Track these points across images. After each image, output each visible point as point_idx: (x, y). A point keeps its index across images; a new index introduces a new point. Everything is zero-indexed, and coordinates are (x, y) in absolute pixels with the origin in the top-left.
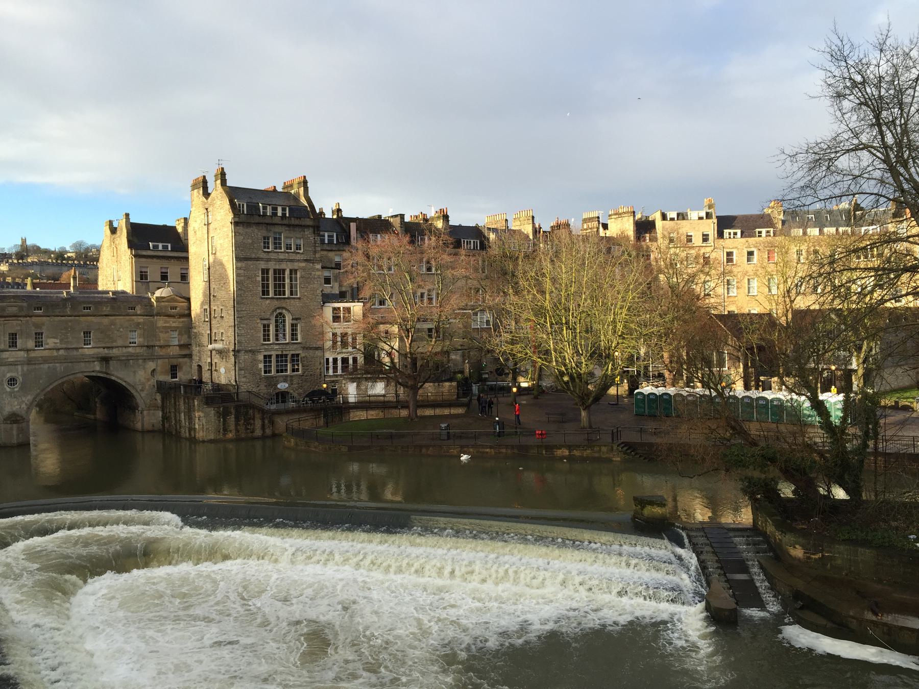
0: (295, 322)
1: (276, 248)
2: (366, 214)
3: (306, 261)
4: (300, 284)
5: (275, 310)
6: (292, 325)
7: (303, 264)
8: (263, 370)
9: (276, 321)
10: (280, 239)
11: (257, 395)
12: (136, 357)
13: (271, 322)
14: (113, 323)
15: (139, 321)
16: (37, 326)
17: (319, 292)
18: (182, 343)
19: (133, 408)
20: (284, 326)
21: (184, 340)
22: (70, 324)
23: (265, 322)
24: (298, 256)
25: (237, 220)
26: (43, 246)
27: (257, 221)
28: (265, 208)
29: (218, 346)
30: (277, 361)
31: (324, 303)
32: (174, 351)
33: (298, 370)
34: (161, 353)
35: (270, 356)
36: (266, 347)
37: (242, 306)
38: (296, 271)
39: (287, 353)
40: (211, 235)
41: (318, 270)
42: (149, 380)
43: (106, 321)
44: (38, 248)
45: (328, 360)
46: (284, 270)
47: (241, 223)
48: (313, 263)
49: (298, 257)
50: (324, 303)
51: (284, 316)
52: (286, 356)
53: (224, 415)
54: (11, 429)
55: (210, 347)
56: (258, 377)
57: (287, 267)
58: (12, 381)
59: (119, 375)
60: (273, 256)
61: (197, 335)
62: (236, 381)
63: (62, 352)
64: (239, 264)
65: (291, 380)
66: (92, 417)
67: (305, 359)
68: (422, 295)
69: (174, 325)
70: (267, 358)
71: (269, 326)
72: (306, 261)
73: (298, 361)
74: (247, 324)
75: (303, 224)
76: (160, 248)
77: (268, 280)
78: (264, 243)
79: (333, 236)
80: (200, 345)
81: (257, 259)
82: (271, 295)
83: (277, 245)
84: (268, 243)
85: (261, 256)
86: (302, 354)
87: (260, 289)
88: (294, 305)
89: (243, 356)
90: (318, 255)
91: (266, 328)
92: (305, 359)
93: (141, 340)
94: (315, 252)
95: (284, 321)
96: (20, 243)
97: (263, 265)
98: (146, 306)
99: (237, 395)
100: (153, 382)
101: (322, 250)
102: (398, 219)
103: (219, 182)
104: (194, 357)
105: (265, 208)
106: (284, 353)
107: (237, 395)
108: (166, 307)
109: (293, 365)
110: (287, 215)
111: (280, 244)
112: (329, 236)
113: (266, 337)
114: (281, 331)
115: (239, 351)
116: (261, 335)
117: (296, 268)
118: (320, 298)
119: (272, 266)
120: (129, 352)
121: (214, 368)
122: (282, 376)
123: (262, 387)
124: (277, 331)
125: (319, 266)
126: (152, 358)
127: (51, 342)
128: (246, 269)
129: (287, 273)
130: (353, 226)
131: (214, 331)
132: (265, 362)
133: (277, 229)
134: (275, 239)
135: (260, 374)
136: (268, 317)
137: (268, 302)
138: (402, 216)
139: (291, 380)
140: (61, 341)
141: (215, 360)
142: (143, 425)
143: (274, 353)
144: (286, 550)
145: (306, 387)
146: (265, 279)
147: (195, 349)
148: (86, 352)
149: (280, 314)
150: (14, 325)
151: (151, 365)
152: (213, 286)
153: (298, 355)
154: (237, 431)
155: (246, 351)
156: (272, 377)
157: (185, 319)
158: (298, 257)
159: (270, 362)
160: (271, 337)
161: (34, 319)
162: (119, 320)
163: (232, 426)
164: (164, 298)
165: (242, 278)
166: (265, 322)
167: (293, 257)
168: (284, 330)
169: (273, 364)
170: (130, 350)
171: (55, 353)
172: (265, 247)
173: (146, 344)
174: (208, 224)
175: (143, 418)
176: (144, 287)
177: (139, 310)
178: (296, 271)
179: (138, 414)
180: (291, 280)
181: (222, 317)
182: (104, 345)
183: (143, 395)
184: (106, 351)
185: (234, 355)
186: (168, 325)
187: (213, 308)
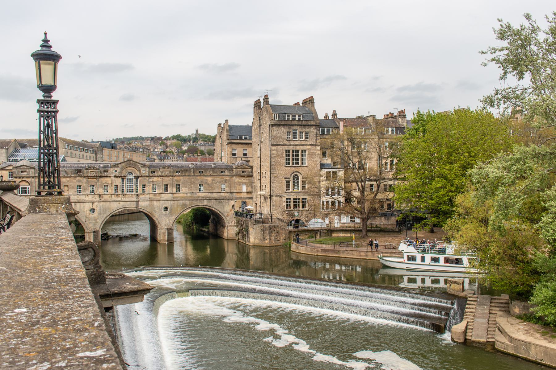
0: (304, 180)
1: (294, 138)
2: (352, 115)
3: (311, 145)
4: (308, 158)
5: (293, 173)
6: (303, 181)
7: (310, 147)
8: (286, 206)
9: (294, 179)
10: (296, 133)
11: (282, 221)
12: (224, 198)
13: (290, 179)
14: (213, 180)
15: (226, 179)
16: (177, 181)
17: (318, 162)
18: (248, 191)
19: (223, 226)
20: (298, 182)
21: (250, 189)
22: (193, 180)
23: (287, 180)
24: (307, 142)
25: (272, 123)
26: (144, 136)
27: (283, 123)
28: (288, 116)
29: (262, 193)
30: (294, 202)
31: (321, 169)
32: (245, 195)
33: (306, 207)
34: (237, 196)
35: (290, 199)
36: (287, 193)
37: (275, 171)
38: (305, 150)
39: (299, 197)
40: (261, 132)
41: (318, 150)
42: (231, 210)
43: (210, 179)
44: (204, 135)
45: (323, 202)
46: (298, 151)
47: (275, 125)
48: (315, 146)
49: (306, 143)
50: (321, 169)
51: (298, 177)
52: (299, 199)
53: (263, 230)
54: (165, 233)
55: (260, 193)
56: (283, 210)
57: (300, 148)
58: (166, 209)
59: (216, 207)
60: (292, 143)
61: (255, 186)
62: (271, 212)
63: (189, 195)
64: (273, 148)
65: (302, 213)
66: (206, 230)
67: (310, 201)
68: (386, 164)
69: (244, 181)
70: (288, 201)
71: (289, 182)
72: (311, 145)
73: (305, 202)
74: (277, 181)
75: (310, 124)
76: (243, 138)
77: (289, 156)
78: (287, 135)
79: (329, 130)
80: (257, 192)
81: (283, 145)
82: (291, 164)
83: (294, 136)
84: (302, 135)
85: (286, 143)
86: (308, 198)
87: (285, 161)
88: (303, 170)
89: (275, 199)
90: (318, 141)
91: (288, 183)
92: (310, 201)
93: (227, 189)
94: (317, 140)
95: (298, 179)
96: (195, 133)
97: (286, 148)
98: (230, 171)
99: (272, 220)
100: (233, 212)
101: (320, 138)
102: (371, 118)
103: (265, 103)
104: (254, 199)
105: (288, 116)
106: (298, 197)
107: (272, 220)
108: (240, 171)
109: (303, 205)
110: (301, 119)
111: (296, 136)
112: (327, 130)
113: (287, 188)
114: (296, 185)
115: (272, 196)
116: (285, 187)
117: (305, 149)
118: (319, 166)
119: (291, 148)
120: (221, 195)
121: (262, 205)
122: (296, 210)
123: (285, 216)
124: (294, 185)
125: (318, 148)
126: (232, 199)
127: (183, 189)
128: (277, 150)
129: (300, 152)
130: (342, 123)
131: (262, 184)
132: (287, 202)
133: (295, 127)
134: (294, 133)
135: (284, 209)
136: (288, 177)
137: (289, 168)
138: (374, 116)
139: (302, 213)
140: (189, 188)
141: (262, 201)
142: (228, 235)
143: (292, 197)
144: (8, 291)
145: (310, 217)
146: (287, 155)
147: (254, 195)
148: (200, 195)
149: (296, 175)
150: (167, 181)
151: (232, 203)
152: (262, 160)
153: (306, 199)
154: (270, 239)
155: (277, 196)
156: (291, 211)
157: (250, 178)
158: (306, 143)
159: (290, 202)
160: (290, 188)
161: (176, 178)
162: (218, 178)
163: (268, 237)
164: (239, 166)
165: (275, 155)
166: (287, 180)
167: (303, 143)
168: (298, 184)
169: (292, 203)
170: (223, 194)
171: (185, 195)
172: (288, 138)
173: (229, 191)
174: (260, 126)
175: (228, 230)
176: (234, 160)
177: (226, 173)
178: (305, 150)
179: (225, 228)
180: (302, 155)
181: (265, 177)
182: (209, 191)
183: (228, 218)
184: (210, 194)
185: (271, 198)
186: (240, 181)
187: (262, 172)
